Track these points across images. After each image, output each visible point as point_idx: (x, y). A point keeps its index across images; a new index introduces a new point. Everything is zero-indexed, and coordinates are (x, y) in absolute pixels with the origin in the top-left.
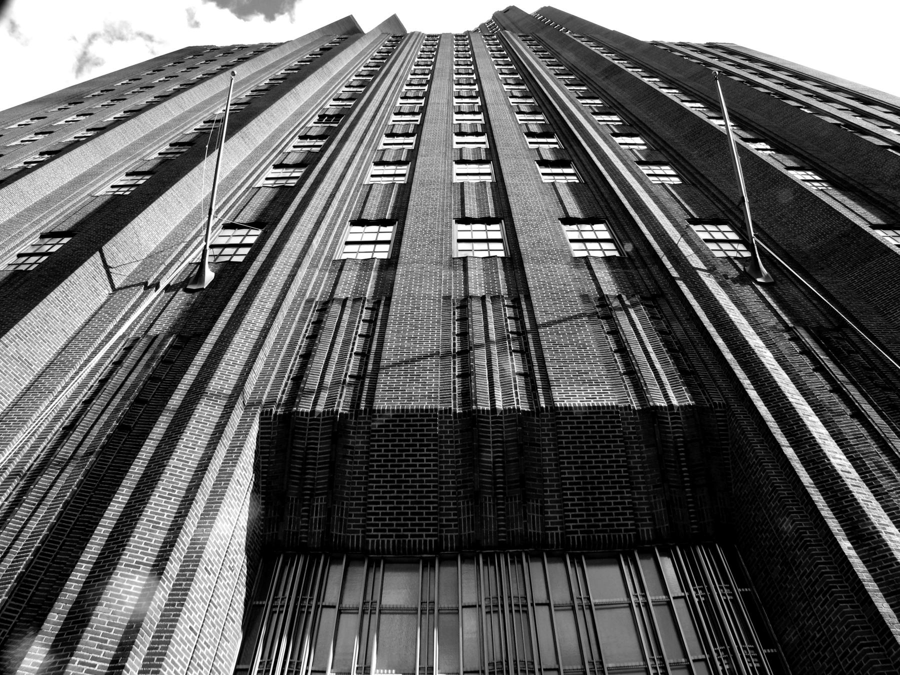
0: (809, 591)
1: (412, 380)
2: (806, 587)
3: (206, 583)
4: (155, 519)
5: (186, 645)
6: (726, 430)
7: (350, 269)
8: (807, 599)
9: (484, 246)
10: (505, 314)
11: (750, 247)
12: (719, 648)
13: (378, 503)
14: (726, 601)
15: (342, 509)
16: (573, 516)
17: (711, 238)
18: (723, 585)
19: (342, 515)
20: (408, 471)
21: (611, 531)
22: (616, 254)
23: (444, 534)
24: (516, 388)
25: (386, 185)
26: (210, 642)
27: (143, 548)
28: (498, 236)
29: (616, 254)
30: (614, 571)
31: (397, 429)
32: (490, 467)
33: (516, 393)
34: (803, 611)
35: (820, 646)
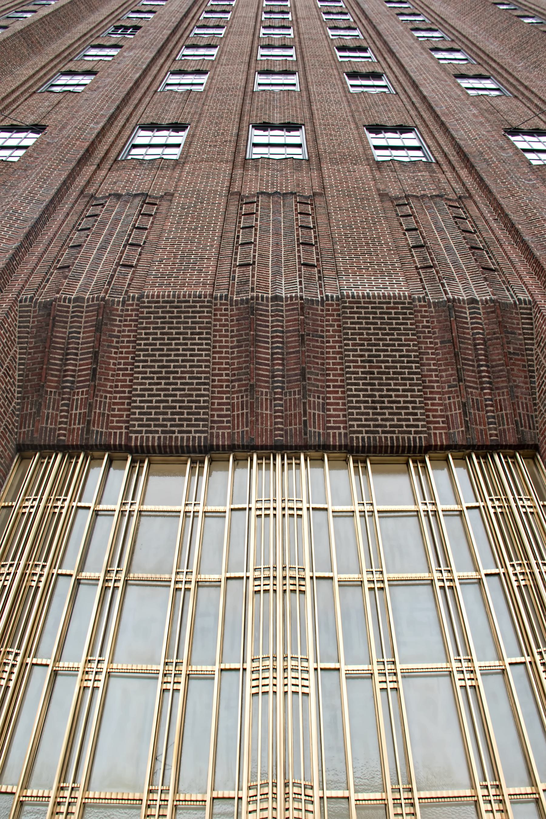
7: (134, 168)
10: (296, 210)
15: (105, 403)
19: (104, 410)
20: (177, 361)
21: (400, 432)
23: (432, 432)
24: (300, 277)
25: (182, 93)
31: (167, 315)
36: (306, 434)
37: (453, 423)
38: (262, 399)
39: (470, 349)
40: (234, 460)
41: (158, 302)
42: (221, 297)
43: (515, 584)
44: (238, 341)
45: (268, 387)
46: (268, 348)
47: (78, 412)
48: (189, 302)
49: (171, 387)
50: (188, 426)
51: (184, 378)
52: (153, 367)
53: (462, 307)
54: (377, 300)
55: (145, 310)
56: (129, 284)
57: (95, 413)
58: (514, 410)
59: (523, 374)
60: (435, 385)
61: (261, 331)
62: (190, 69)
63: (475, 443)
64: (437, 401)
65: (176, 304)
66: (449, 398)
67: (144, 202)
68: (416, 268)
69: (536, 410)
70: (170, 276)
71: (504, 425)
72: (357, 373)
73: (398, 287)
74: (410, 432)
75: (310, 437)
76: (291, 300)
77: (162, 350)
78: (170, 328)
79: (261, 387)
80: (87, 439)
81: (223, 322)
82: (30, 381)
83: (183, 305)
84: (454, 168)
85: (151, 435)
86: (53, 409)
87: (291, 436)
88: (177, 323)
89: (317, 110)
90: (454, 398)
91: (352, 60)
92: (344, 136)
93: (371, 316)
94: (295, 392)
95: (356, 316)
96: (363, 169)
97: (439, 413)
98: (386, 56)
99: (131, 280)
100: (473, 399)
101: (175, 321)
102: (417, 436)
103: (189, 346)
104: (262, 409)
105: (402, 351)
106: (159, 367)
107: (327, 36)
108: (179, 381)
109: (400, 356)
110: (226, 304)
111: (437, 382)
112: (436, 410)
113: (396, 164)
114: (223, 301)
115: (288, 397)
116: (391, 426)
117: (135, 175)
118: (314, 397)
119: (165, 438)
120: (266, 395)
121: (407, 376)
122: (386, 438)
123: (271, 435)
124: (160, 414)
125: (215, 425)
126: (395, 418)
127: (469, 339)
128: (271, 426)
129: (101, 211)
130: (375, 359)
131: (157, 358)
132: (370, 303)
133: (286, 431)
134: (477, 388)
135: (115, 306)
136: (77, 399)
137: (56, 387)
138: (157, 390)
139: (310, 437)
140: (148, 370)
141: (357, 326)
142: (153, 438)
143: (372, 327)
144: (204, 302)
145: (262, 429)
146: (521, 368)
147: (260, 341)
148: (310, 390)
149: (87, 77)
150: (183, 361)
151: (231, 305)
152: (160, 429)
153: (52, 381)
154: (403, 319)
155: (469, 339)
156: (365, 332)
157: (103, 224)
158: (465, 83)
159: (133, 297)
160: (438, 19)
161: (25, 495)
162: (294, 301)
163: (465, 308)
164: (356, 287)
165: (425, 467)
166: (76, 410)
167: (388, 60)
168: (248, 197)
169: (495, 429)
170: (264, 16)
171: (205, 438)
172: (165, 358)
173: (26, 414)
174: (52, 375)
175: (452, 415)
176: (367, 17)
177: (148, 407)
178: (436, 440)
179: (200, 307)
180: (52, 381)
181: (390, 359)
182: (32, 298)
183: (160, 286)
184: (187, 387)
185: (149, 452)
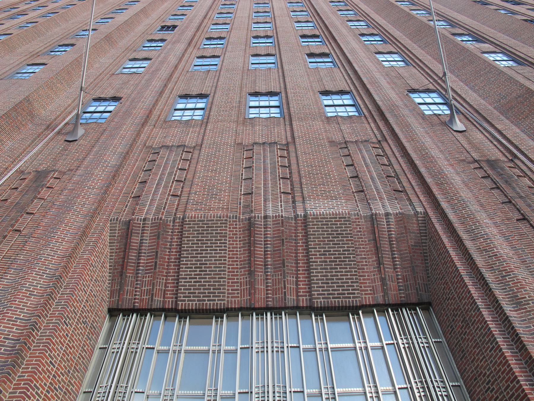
0: (481, 340)
1: (211, 198)
2: (479, 338)
3: (65, 332)
4: (31, 289)
5: (46, 374)
6: (426, 230)
7: (176, 127)
8: (479, 347)
9: (267, 110)
10: (277, 154)
11: (450, 107)
12: (417, 380)
13: (186, 278)
14: (423, 347)
15: (163, 282)
16: (317, 287)
17: (423, 102)
18: (422, 336)
19: (162, 287)
20: (207, 257)
21: (343, 298)
22: (356, 114)
23: (364, 296)
24: (281, 202)
25: (204, 72)
26: (65, 372)
27: (21, 309)
28: (252, 111)
29: (356, 114)
30: (345, 325)
31: (200, 229)
32: (261, 255)
33: (281, 205)
34: (477, 355)
35: (490, 381)
36: (285, 300)
37: (376, 290)
38: (258, 279)
39: (387, 244)
40: (242, 316)
41: (195, 221)
42: (233, 216)
43: (417, 395)
44: (243, 244)
45: (262, 272)
46: (262, 248)
47: (146, 288)
48: (213, 220)
49: (203, 273)
50: (213, 296)
51: (211, 267)
52: (192, 261)
53: (381, 218)
54: (329, 217)
55: (187, 226)
56: (177, 209)
57: (156, 289)
58: (415, 281)
59: (421, 258)
60: (365, 267)
61: (257, 237)
62: (208, 55)
63: (390, 303)
64: (366, 277)
65: (205, 222)
66: (374, 275)
67: (183, 151)
68: (353, 192)
69: (429, 281)
70: (201, 203)
71: (409, 290)
72: (317, 262)
73: (341, 207)
74: (350, 298)
75: (288, 302)
76: (276, 218)
77: (198, 250)
78: (202, 237)
79: (257, 272)
80: (151, 305)
81: (234, 232)
82: (116, 269)
83: (210, 222)
84: (376, 121)
85: (191, 303)
86: (131, 286)
87: (276, 301)
88: (207, 234)
89: (289, 82)
90: (377, 275)
91: (310, 43)
92: (306, 100)
93: (325, 227)
94: (278, 274)
95: (316, 227)
96: (318, 124)
97: (368, 285)
98: (331, 41)
99: (178, 205)
100: (389, 275)
101: (205, 232)
102: (354, 300)
103: (214, 248)
104: (258, 285)
105: (344, 247)
106: (195, 261)
107: (294, 28)
108: (208, 269)
109: (343, 251)
110: (236, 221)
111: (367, 265)
112: (366, 283)
113: (339, 119)
114: (234, 220)
115: (274, 278)
116: (338, 294)
117: (177, 131)
118: (290, 277)
119: (199, 304)
120: (261, 277)
121: (347, 263)
122: (335, 301)
123: (264, 301)
124: (196, 289)
125: (230, 296)
126: (341, 289)
127: (386, 238)
128: (264, 295)
129: (157, 158)
130: (327, 253)
131: (195, 255)
132: (324, 218)
133: (273, 299)
134: (391, 268)
135: (168, 223)
136: (146, 281)
137: (132, 273)
138: (195, 275)
139: (288, 302)
140: (189, 263)
141: (316, 233)
142: (192, 304)
143: (326, 233)
144: (223, 220)
145: (258, 297)
146: (419, 254)
147: (257, 244)
148: (288, 273)
149: (145, 62)
150: (210, 257)
151: (239, 222)
152: (196, 299)
153: (130, 270)
154: (345, 227)
155: (386, 238)
156: (321, 236)
157: (159, 166)
158: (381, 58)
159: (180, 218)
160: (364, 14)
161: (114, 341)
162: (278, 218)
163: (383, 219)
164: (316, 208)
165: (359, 319)
166: (145, 287)
167: (333, 44)
168: (247, 146)
169: (403, 293)
170: (254, 14)
171: (224, 304)
172: (199, 256)
173: (114, 290)
174: (130, 266)
175: (376, 286)
176: (318, 15)
177: (189, 286)
178: (366, 302)
179: (221, 224)
180: (130, 270)
181: (337, 253)
182: (117, 218)
183: (196, 210)
184: (212, 273)
185: (189, 312)
